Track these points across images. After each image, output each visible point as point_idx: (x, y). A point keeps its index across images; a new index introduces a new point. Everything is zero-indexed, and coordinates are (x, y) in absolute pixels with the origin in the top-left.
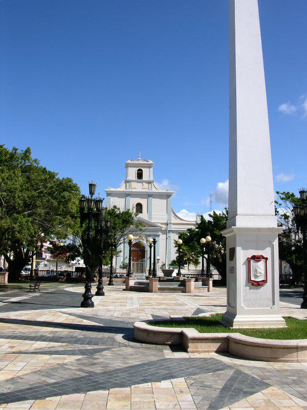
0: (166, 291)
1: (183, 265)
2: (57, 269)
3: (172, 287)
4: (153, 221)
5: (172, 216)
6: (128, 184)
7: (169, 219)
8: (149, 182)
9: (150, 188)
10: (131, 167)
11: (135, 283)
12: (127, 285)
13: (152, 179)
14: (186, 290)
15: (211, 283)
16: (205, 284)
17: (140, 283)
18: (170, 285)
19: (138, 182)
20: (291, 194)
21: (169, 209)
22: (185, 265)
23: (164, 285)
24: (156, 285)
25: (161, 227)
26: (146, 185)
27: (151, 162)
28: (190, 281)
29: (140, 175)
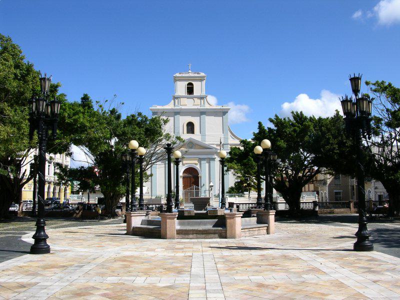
0: (191, 236)
1: (242, 192)
2: (89, 201)
3: (201, 228)
4: (207, 142)
5: (229, 137)
6: (176, 101)
7: (226, 139)
8: (201, 98)
9: (203, 104)
10: (180, 80)
11: (143, 222)
12: (129, 225)
13: (204, 94)
14: (226, 232)
15: (272, 218)
16: (262, 220)
17: (149, 222)
18: (200, 224)
19: (188, 98)
20: (386, 84)
21: (226, 128)
22: (245, 193)
23: (188, 224)
24: (174, 225)
25: (216, 149)
26: (197, 101)
27: (202, 74)
28: (233, 216)
29: (190, 90)
